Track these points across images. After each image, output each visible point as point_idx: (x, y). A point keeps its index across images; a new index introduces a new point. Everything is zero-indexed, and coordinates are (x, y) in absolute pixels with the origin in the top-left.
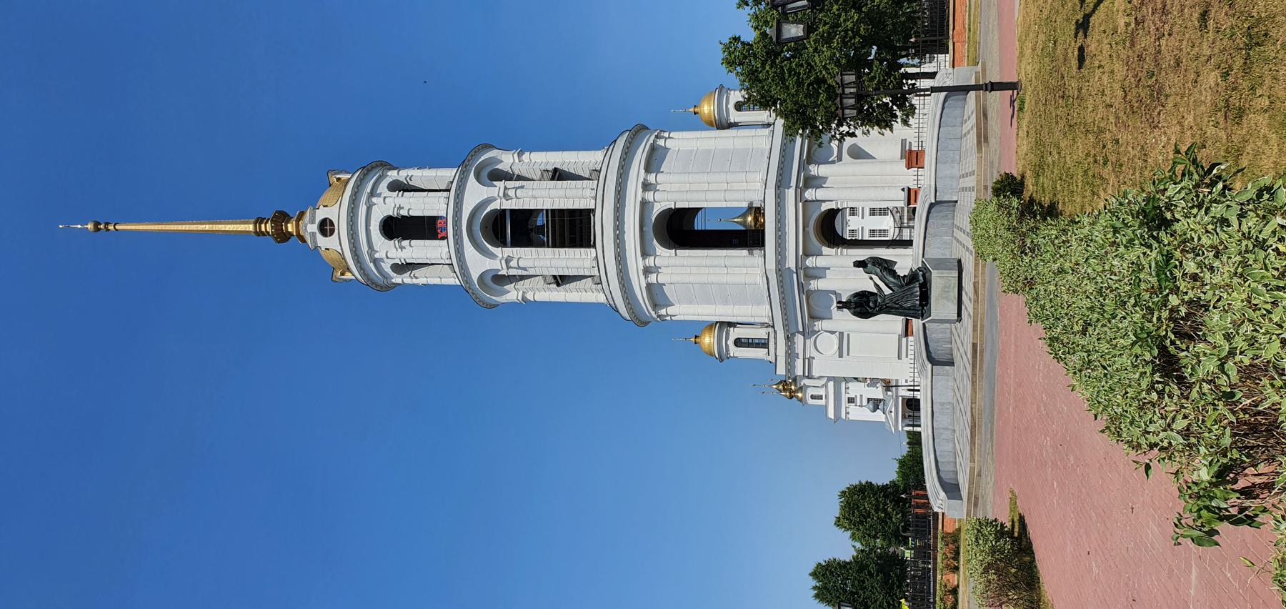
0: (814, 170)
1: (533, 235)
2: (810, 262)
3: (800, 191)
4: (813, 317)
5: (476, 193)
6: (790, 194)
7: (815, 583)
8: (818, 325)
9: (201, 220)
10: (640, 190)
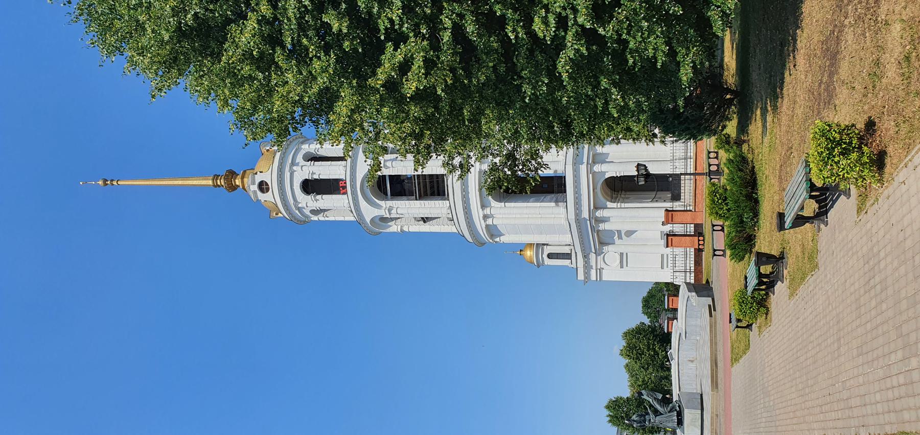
0: (599, 214)
2: (599, 214)
3: (590, 166)
6: (583, 168)
7: (607, 412)
8: (605, 248)
9: (175, 178)
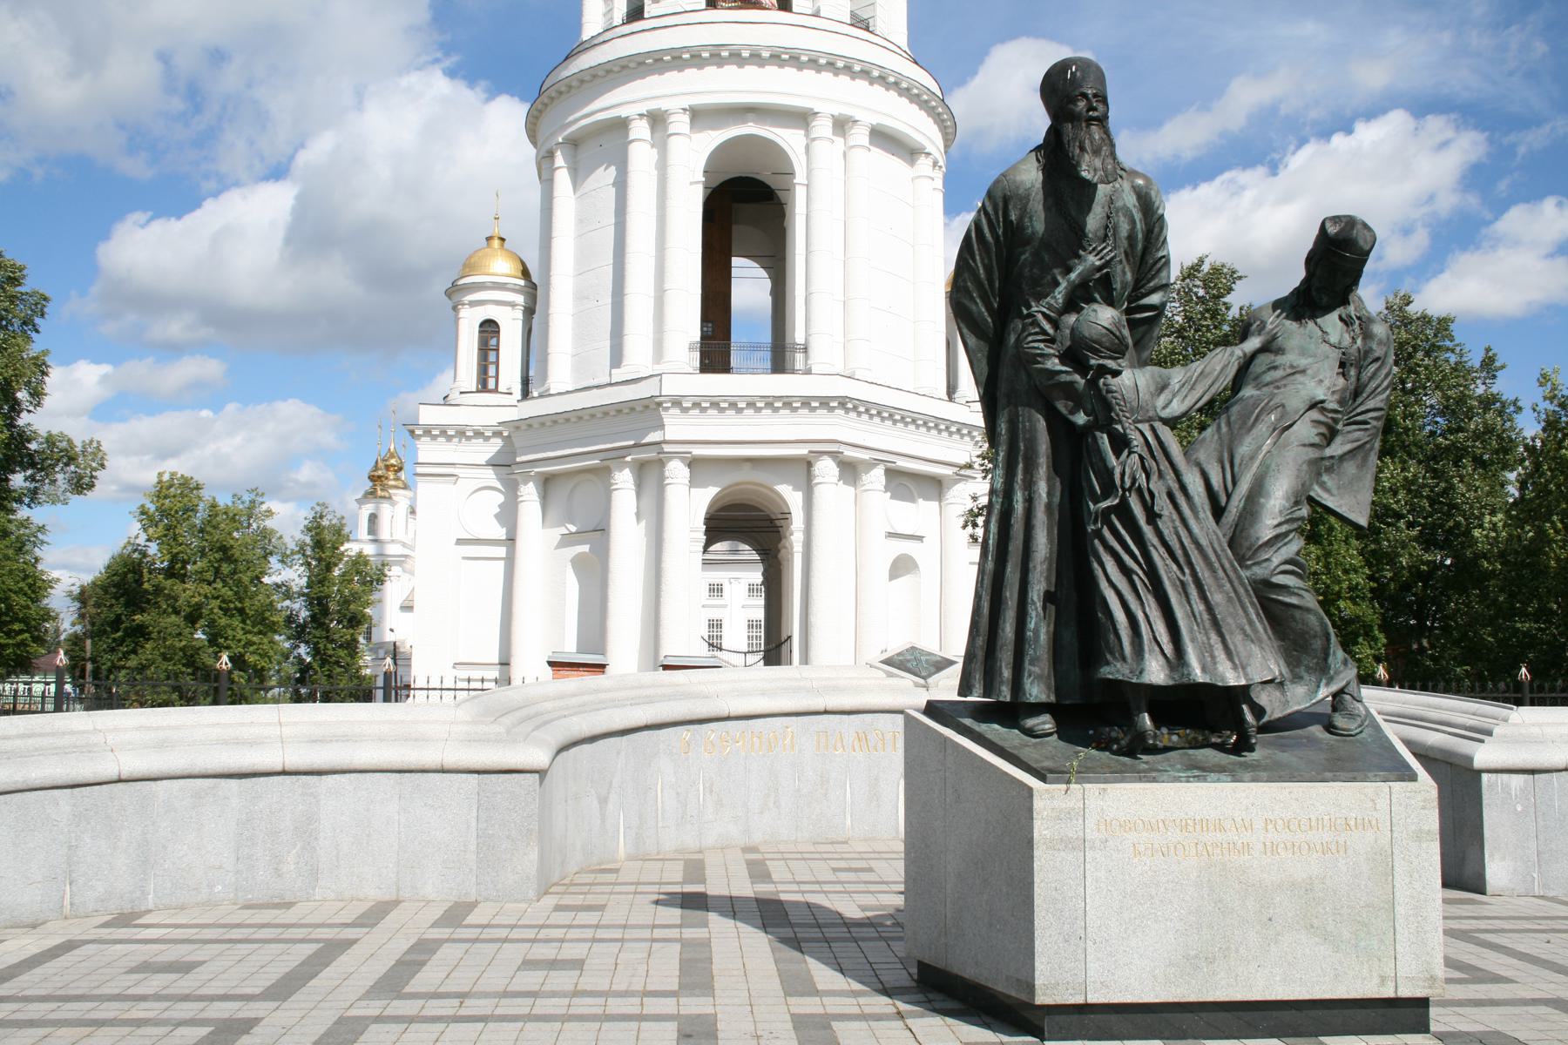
4: (547, 483)
8: (529, 493)
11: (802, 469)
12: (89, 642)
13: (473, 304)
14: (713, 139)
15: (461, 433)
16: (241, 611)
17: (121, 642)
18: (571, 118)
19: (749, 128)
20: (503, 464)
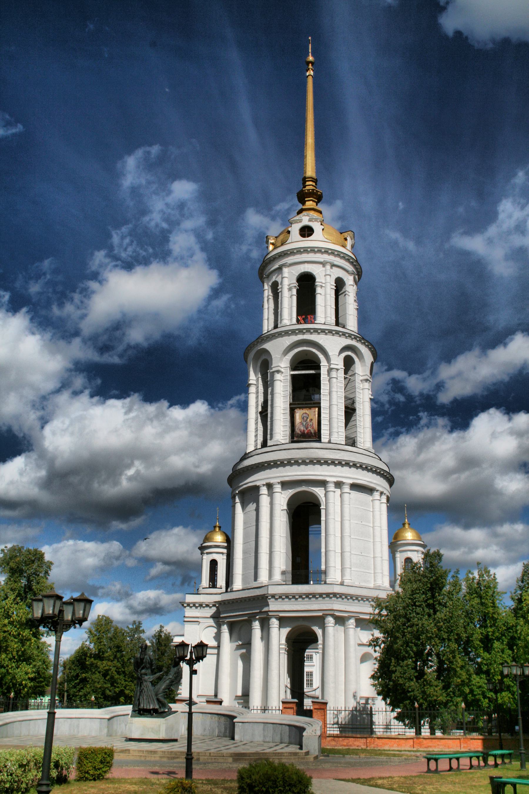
1: (304, 392)
5: (334, 345)
8: (225, 629)
10: (335, 480)
11: (320, 621)
12: (66, 684)
13: (208, 553)
14: (290, 492)
15: (201, 605)
16: (124, 672)
17: (79, 684)
18: (241, 484)
19: (304, 488)
20: (216, 617)
